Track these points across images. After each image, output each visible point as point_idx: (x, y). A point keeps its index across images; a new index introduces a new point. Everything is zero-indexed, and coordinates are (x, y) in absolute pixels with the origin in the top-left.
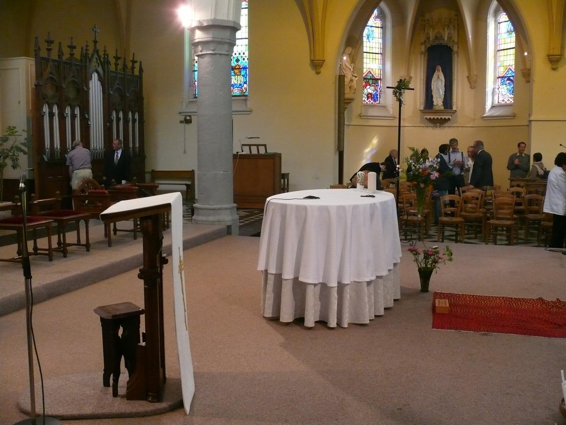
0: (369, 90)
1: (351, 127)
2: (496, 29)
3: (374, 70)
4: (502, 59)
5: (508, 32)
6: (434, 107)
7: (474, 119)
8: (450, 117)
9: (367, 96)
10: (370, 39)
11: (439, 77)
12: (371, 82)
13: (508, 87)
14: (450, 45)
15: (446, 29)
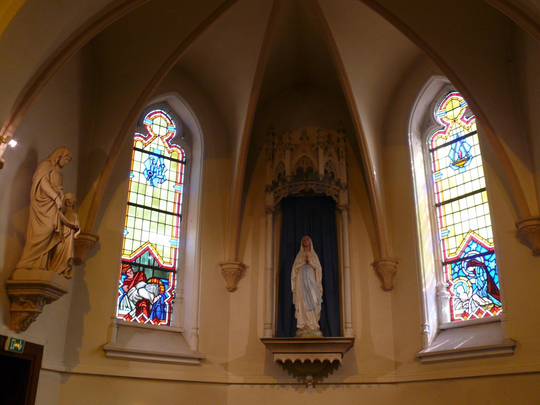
0: (145, 291)
1: (72, 377)
2: (428, 162)
3: (159, 248)
4: (448, 221)
5: (455, 163)
6: (298, 333)
7: (397, 364)
8: (338, 357)
9: (137, 305)
10: (155, 181)
11: (307, 262)
12: (149, 273)
13: (473, 281)
14: (330, 192)
15: (321, 151)
